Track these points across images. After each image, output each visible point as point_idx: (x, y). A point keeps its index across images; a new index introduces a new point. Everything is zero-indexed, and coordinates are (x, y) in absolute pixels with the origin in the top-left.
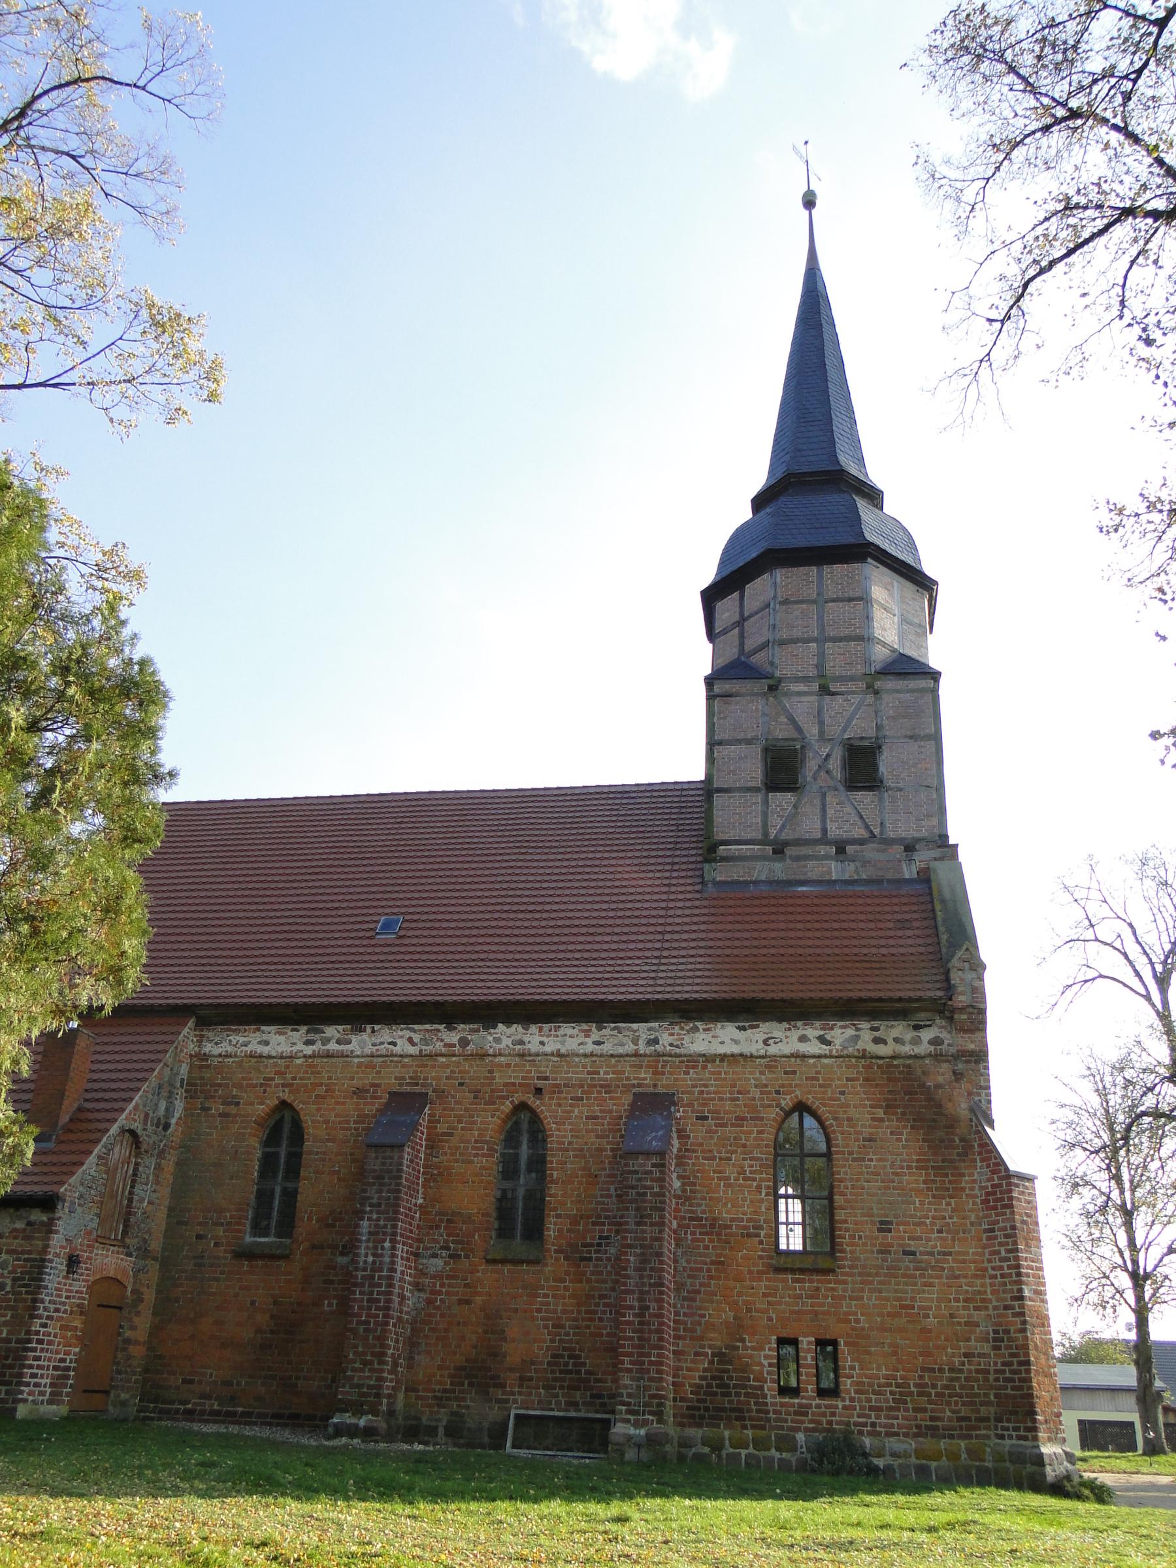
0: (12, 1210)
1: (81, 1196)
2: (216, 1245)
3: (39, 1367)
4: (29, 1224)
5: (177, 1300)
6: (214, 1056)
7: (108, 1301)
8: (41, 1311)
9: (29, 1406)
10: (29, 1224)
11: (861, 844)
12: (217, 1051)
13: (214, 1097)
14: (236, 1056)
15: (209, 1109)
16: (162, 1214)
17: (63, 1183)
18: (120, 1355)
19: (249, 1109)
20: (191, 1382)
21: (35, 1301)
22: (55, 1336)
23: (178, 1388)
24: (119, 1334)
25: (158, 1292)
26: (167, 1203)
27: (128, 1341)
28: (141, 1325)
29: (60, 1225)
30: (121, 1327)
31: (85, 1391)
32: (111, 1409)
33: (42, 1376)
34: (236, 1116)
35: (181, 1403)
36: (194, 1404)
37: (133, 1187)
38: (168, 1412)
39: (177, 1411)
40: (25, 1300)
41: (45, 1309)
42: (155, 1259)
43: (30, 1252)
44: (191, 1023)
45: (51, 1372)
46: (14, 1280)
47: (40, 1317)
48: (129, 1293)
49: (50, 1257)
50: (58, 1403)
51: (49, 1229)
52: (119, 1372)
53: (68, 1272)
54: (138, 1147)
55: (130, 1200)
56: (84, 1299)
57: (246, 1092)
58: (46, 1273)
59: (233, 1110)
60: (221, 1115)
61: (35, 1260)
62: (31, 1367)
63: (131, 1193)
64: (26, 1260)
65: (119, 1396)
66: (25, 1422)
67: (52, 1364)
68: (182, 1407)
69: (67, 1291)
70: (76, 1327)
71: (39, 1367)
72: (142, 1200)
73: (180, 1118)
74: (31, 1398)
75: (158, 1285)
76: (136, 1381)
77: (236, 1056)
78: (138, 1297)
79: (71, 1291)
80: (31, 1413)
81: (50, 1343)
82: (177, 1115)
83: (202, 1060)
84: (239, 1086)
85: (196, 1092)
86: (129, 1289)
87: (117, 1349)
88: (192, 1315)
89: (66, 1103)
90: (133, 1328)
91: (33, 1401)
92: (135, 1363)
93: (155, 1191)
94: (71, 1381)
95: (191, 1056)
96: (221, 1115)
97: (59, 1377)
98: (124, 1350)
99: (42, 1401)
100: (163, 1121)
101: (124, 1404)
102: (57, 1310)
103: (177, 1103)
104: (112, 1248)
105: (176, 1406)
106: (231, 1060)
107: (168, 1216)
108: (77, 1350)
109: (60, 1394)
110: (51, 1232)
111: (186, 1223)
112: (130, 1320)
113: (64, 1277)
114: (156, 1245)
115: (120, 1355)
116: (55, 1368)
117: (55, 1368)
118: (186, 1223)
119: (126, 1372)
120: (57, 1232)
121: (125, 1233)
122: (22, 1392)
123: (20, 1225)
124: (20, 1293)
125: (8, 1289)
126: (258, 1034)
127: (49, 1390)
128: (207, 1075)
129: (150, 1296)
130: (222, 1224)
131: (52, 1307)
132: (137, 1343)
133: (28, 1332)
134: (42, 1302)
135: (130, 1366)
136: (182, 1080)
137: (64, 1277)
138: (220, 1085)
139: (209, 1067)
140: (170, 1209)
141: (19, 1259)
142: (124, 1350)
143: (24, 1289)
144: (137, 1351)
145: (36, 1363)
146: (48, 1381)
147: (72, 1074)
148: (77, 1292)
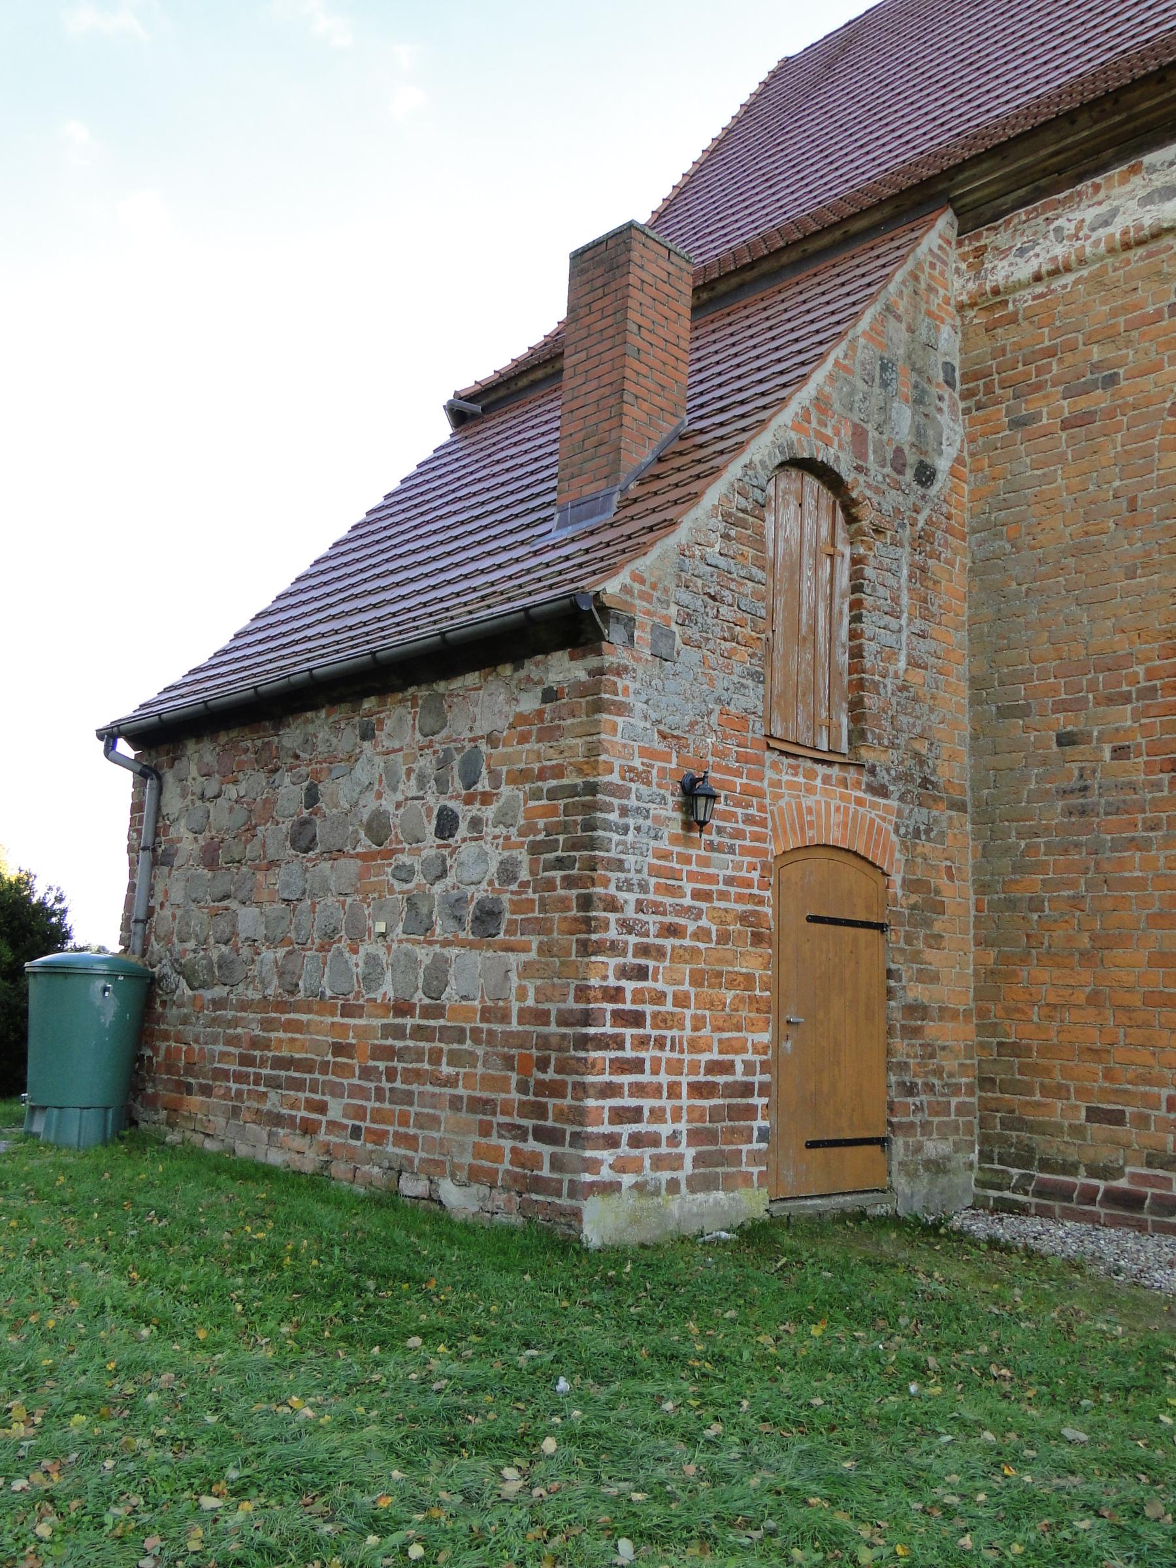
0: (506, 670)
1: (687, 618)
2: (1120, 752)
3: (639, 1090)
4: (550, 695)
5: (1035, 905)
6: (1020, 285)
7: (840, 914)
8: (613, 933)
9: (627, 1201)
10: (550, 695)
11: (860, 1216)
12: (1025, 270)
13: (1039, 387)
14: (1082, 262)
15: (1035, 417)
16: (955, 698)
17: (611, 570)
18: (900, 1045)
19: (1147, 383)
20: (1116, 1118)
21: (586, 903)
22: (681, 1001)
23: (1077, 1130)
24: (890, 993)
25: (982, 888)
26: (963, 669)
27: (916, 1010)
28: (949, 971)
29: (627, 689)
30: (890, 974)
31: (812, 1145)
32: (900, 1182)
33: (657, 1115)
34: (1110, 414)
35: (1093, 1172)
36: (1134, 1177)
37: (856, 619)
38: (1064, 1193)
39: (1089, 1196)
40: (563, 904)
41: (627, 926)
42: (960, 807)
43: (558, 771)
44: (944, 223)
45: (685, 1102)
46: (535, 849)
47: (614, 948)
48: (897, 889)
49: (615, 778)
50: (729, 1183)
51: (594, 699)
52: (910, 1090)
53: (687, 826)
54: (851, 519)
55: (857, 653)
56: (761, 902)
57: (1129, 343)
58: (607, 826)
59: (1100, 399)
60: (1066, 425)
61: (572, 791)
62: (610, 1090)
63: (854, 635)
64: (553, 794)
65: (919, 1149)
66: (614, 1254)
67: (684, 1080)
68: (1102, 1185)
69: (692, 877)
70: (749, 978)
71: (639, 1090)
72: (890, 655)
73: (959, 460)
74: (628, 1179)
75: (976, 868)
76: (962, 1109)
77: (1082, 262)
78: (930, 906)
79: (712, 879)
80: (635, 1221)
81: (662, 1021)
82: (950, 452)
83: (990, 309)
84: (1107, 336)
85: (989, 390)
86: (897, 878)
87: (890, 1032)
88: (1085, 941)
89: (634, 412)
90: (928, 977)
91: (639, 1187)
92: (950, 1064)
93: (922, 635)
94: (760, 1123)
95: (961, 307)
96: (1066, 425)
97: (715, 1114)
98: (916, 1032)
99: (673, 1186)
100: (912, 458)
101: (937, 1167)
102: (672, 931)
103: (944, 419)
104: (821, 769)
105: (1081, 1179)
106: (1069, 279)
107: (975, 701)
108: (765, 1037)
109: (734, 1158)
110: (598, 707)
111: (1023, 711)
112: (916, 957)
113: (674, 840)
114: (954, 768)
115: (900, 1045)
116: (698, 1090)
117: (698, 1090)
118: (1023, 711)
119: (930, 1088)
120: (622, 709)
121: (858, 736)
122: (593, 1166)
123: (530, 703)
124: (550, 885)
125: (524, 875)
126: (1136, 180)
127: (690, 1153)
128: (1008, 337)
129: (960, 896)
130: (1126, 698)
131: (652, 921)
132: (944, 1013)
133: (582, 992)
134: (612, 905)
135: (938, 1072)
136: (949, 368)
137: (674, 840)
138: (1050, 353)
139: (1013, 319)
140: (976, 683)
141: (536, 795)
142: (913, 1032)
143: (558, 874)
144: (954, 1037)
145: (626, 1079)
146: (683, 1126)
147: (634, 339)
148: (729, 881)
